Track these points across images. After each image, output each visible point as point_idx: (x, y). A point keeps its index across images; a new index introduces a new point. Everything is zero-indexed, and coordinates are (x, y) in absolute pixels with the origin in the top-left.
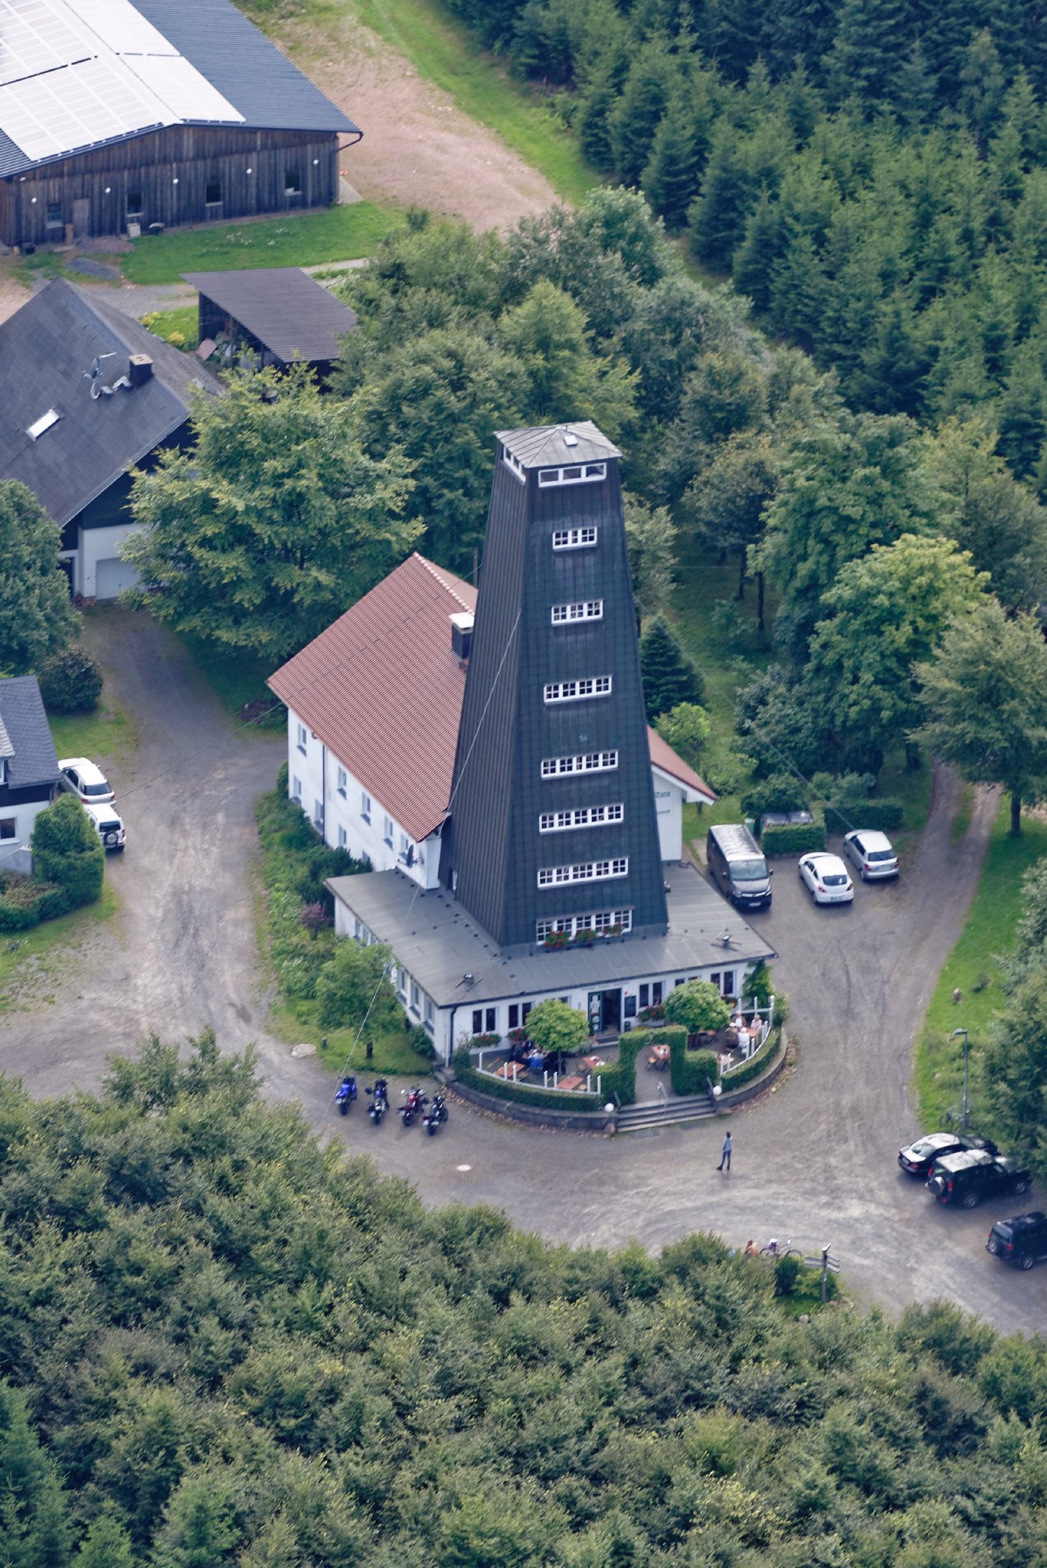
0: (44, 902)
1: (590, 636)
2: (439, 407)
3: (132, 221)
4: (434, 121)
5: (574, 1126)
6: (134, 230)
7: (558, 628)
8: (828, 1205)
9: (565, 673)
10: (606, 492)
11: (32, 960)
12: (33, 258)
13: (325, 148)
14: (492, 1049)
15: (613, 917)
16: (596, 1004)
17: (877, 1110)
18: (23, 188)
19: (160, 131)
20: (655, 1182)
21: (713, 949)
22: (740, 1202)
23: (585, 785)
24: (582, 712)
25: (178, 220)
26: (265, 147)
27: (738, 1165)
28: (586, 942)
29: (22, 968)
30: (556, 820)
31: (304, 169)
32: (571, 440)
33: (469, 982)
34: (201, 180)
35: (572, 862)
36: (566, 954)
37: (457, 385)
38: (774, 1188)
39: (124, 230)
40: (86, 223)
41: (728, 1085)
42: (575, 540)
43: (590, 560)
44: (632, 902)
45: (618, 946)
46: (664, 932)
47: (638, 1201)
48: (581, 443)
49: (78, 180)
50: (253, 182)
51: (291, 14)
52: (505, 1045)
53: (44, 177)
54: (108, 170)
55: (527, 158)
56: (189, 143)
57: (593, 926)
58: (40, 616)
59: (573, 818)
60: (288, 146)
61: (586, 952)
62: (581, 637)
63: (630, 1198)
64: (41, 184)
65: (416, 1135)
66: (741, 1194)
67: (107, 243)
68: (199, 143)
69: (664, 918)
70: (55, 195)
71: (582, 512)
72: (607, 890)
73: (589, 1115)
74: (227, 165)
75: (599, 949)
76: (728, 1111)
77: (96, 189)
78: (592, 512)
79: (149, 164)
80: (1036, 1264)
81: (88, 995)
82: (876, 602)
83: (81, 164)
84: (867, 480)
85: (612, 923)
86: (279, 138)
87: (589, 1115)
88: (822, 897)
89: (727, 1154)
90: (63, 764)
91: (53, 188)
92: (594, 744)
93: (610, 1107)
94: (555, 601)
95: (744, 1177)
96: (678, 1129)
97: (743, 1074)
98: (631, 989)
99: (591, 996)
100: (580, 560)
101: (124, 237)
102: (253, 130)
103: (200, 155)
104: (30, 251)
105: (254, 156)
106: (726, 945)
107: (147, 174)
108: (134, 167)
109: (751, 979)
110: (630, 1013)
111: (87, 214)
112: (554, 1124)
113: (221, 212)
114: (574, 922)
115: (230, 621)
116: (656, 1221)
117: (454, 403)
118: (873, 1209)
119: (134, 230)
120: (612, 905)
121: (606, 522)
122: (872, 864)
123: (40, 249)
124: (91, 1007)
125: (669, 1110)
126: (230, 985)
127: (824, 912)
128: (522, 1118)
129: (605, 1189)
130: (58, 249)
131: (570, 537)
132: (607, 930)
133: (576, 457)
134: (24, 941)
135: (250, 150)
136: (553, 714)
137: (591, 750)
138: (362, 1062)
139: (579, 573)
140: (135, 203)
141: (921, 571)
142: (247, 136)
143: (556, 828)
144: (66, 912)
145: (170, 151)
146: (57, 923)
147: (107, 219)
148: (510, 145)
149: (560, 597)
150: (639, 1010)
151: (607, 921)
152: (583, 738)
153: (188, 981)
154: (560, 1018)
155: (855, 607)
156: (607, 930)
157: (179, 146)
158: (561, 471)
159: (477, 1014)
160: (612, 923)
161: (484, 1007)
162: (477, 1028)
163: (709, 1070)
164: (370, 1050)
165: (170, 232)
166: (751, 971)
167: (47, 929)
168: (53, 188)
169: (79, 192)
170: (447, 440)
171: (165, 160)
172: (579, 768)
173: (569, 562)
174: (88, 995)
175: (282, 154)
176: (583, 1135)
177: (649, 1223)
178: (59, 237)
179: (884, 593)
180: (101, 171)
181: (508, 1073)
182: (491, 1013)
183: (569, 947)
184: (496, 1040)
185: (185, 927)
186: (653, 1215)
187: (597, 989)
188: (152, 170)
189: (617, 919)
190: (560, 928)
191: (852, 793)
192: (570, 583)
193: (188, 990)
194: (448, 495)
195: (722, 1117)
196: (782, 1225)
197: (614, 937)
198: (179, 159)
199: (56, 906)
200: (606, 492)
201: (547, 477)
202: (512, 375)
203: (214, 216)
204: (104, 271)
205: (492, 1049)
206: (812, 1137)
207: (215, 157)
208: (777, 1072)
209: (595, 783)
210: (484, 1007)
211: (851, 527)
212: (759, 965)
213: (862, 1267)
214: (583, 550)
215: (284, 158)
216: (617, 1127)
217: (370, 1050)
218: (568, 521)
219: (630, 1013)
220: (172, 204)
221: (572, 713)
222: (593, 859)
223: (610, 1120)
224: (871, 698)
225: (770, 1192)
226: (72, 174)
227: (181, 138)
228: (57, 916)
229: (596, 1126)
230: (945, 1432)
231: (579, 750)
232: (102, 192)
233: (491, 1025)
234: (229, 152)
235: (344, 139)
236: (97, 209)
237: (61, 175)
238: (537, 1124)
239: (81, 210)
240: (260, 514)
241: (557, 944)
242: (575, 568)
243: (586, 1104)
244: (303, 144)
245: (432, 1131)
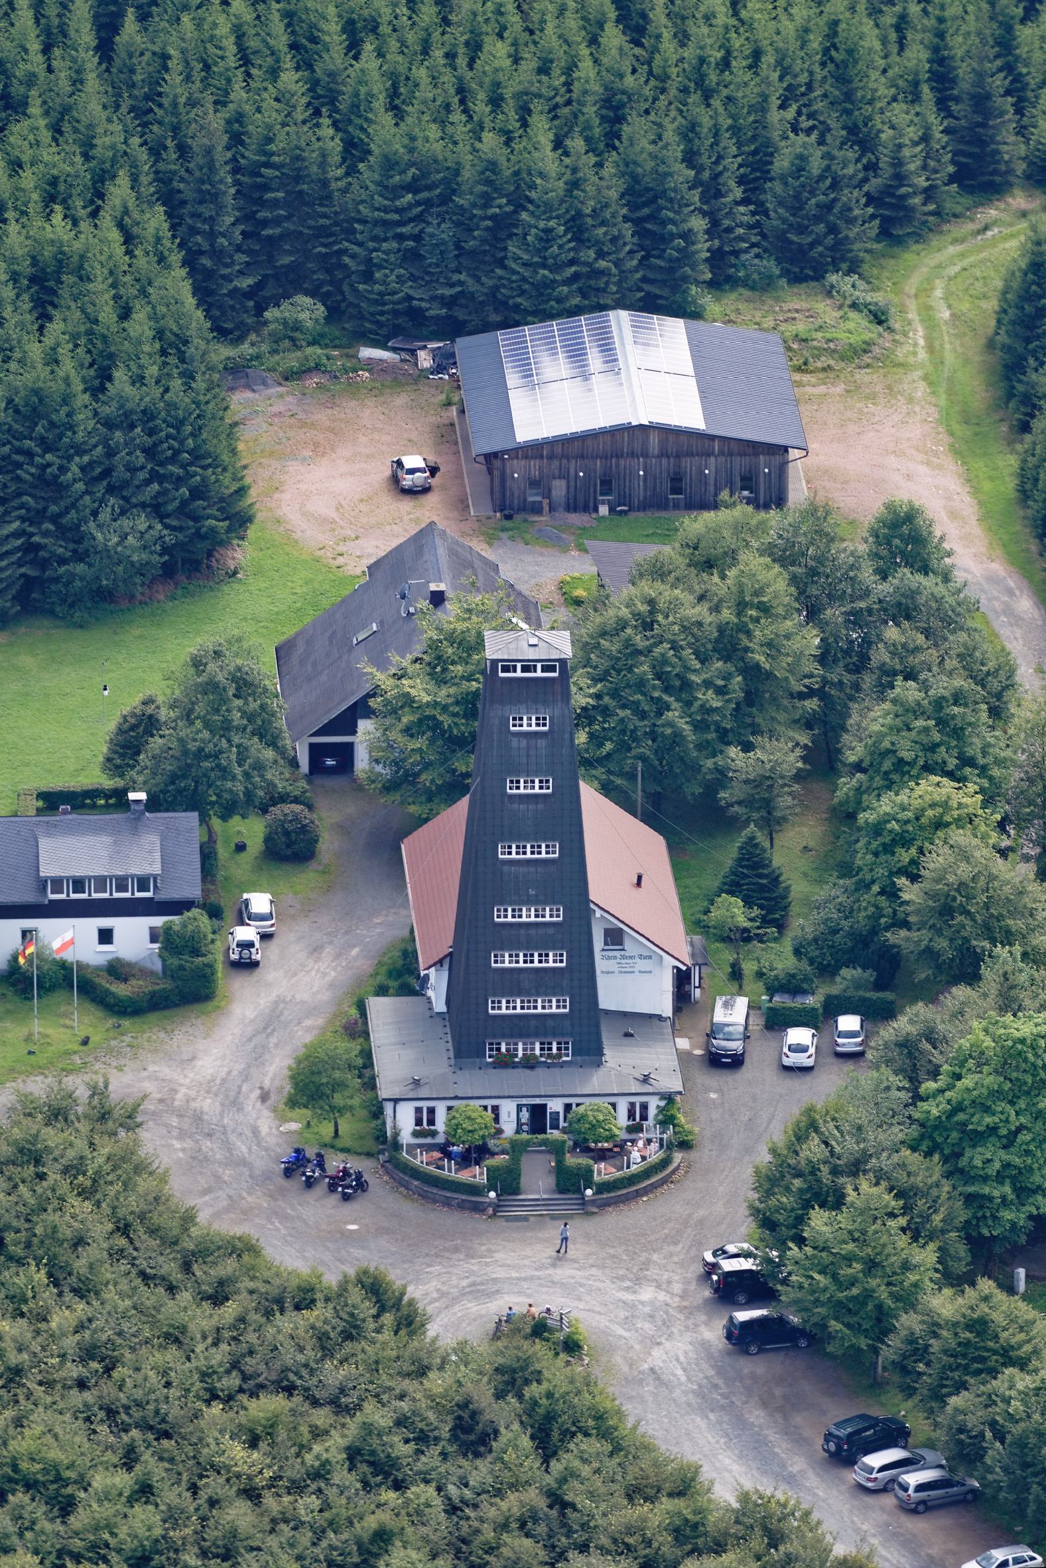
0: (153, 994)
1: (540, 806)
2: (628, 643)
3: (603, 503)
4: (921, 457)
5: (462, 1206)
6: (604, 510)
7: (512, 796)
8: (627, 1289)
9: (516, 835)
10: (558, 688)
11: (127, 1039)
12: (508, 524)
13: (777, 459)
14: (429, 1140)
15: (554, 1046)
16: (525, 1115)
17: (719, 1223)
18: (508, 465)
19: (628, 429)
20: (498, 1256)
21: (633, 1082)
22: (556, 1278)
23: (532, 932)
24: (532, 869)
25: (644, 507)
26: (722, 453)
27: (573, 1251)
28: (530, 1063)
29: (113, 1043)
30: (507, 958)
31: (757, 477)
32: (534, 641)
33: (417, 1083)
34: (665, 475)
35: (519, 995)
36: (510, 1071)
37: (648, 625)
38: (594, 1271)
39: (596, 510)
40: (563, 500)
41: (603, 1188)
42: (529, 725)
43: (542, 743)
44: (571, 1035)
45: (557, 1070)
46: (599, 1064)
47: (475, 1268)
48: (541, 644)
49: (556, 463)
50: (712, 481)
51: (868, 366)
52: (440, 1139)
53: (526, 457)
54: (582, 457)
55: (975, 491)
56: (654, 441)
57: (537, 1052)
58: (238, 770)
59: (521, 958)
60: (742, 454)
61: (528, 1072)
62: (531, 807)
63: (473, 1265)
64: (523, 463)
65: (334, 1199)
66: (563, 1273)
67: (576, 519)
68: (663, 444)
69: (600, 1053)
70: (536, 474)
71: (536, 702)
72: (550, 1023)
73: (474, 1199)
74: (688, 464)
75: (539, 1071)
76: (595, 1210)
77: (572, 472)
78: (545, 703)
79: (619, 456)
80: (761, 1351)
81: (151, 1068)
82: (889, 826)
83: (558, 449)
84: (926, 730)
85: (555, 1051)
86: (733, 445)
87: (474, 1199)
88: (787, 1062)
89: (565, 1239)
90: (245, 896)
91: (535, 467)
92: (541, 897)
93: (492, 1194)
94: (510, 773)
95: (575, 1261)
96: (547, 1219)
97: (615, 1181)
98: (555, 1106)
99: (519, 1108)
100: (533, 742)
101: (594, 515)
102: (713, 438)
103: (663, 454)
104: (508, 517)
105: (712, 459)
106: (646, 1079)
107: (618, 465)
108: (605, 457)
109: (661, 1110)
110: (555, 1126)
111: (564, 492)
112: (447, 1203)
113: (682, 504)
114: (520, 1046)
115: (424, 798)
116: (482, 1284)
117: (639, 641)
118: (662, 1296)
119: (604, 510)
120: (554, 1035)
121: (557, 712)
122: (840, 1041)
123: (518, 518)
124: (149, 1077)
125: (546, 1203)
126: (270, 1075)
127: (787, 1074)
128: (424, 1196)
129: (455, 1256)
130: (536, 518)
131: (525, 722)
132: (550, 1056)
133: (531, 654)
134: (126, 1023)
135: (709, 454)
136: (506, 868)
137: (535, 900)
138: (327, 1139)
139: (532, 752)
140: (607, 485)
141: (933, 805)
142: (707, 442)
143: (507, 965)
144: (176, 1005)
145: (637, 446)
146: (166, 1013)
147: (581, 498)
148: (969, 481)
149: (515, 769)
150: (562, 1124)
151: (550, 1049)
152: (532, 892)
153: (240, 1066)
154: (469, 1118)
155: (877, 829)
156: (550, 1056)
157: (645, 444)
158: (539, 666)
159: (418, 1110)
160: (555, 1051)
161: (425, 1105)
162: (419, 1122)
163: (586, 1176)
164: (336, 1131)
165: (633, 516)
166: (663, 1103)
167: (153, 1017)
168: (535, 467)
169: (557, 473)
170: (630, 670)
171: (633, 455)
172: (528, 916)
173: (524, 743)
174: (151, 1068)
175: (737, 460)
176: (466, 1214)
177: (473, 1284)
178: (537, 509)
179: (898, 821)
180: (576, 457)
181: (420, 1160)
182: (431, 1111)
183: (515, 1066)
184: (434, 1134)
185: (265, 1028)
186: (479, 1280)
187: (524, 1101)
188: (622, 462)
189: (559, 1049)
190: (508, 1050)
191: (858, 985)
192: (524, 760)
193: (235, 1073)
194: (622, 713)
195: (589, 1214)
196: (579, 1299)
197: (554, 1063)
198: (646, 455)
199: (167, 998)
200: (558, 688)
201: (506, 669)
202: (700, 624)
203: (676, 506)
204: (559, 538)
205: (429, 1140)
206: (652, 1238)
207: (678, 456)
208: (654, 1187)
209: (541, 931)
210: (425, 1105)
211: (906, 768)
212: (669, 1098)
213: (621, 1337)
214: (536, 733)
215: (740, 464)
216: (495, 1211)
217: (336, 1131)
218: (523, 708)
219: (555, 1126)
220: (639, 492)
221: (523, 870)
222: (538, 995)
223: (490, 1204)
224: (877, 907)
225: (587, 1273)
226: (551, 457)
227: (648, 437)
228: (166, 1008)
229: (478, 1208)
230: (472, 1437)
231: (529, 902)
232: (576, 475)
233: (431, 1122)
234: (690, 454)
235: (794, 454)
236: (572, 490)
237: (542, 457)
238: (435, 1201)
239: (559, 489)
240: (445, 708)
241: (505, 1063)
242: (528, 748)
243: (474, 1190)
244: (757, 455)
245: (346, 1198)
